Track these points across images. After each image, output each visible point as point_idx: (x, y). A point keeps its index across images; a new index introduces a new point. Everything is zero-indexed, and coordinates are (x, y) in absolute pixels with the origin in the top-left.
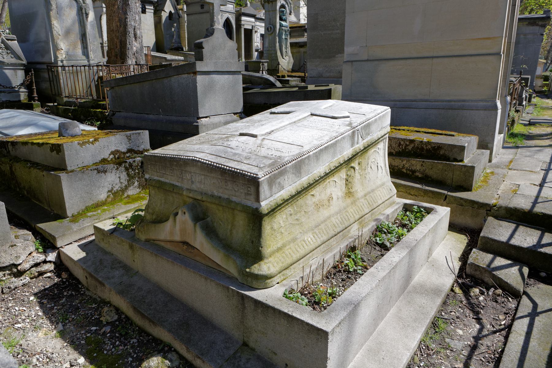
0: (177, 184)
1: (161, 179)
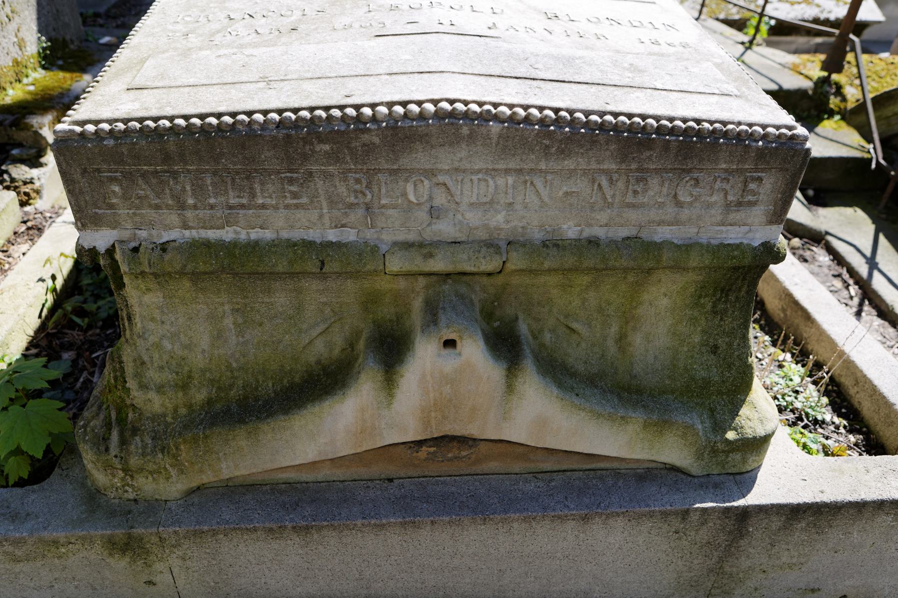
0: (332, 236)
1: (212, 234)
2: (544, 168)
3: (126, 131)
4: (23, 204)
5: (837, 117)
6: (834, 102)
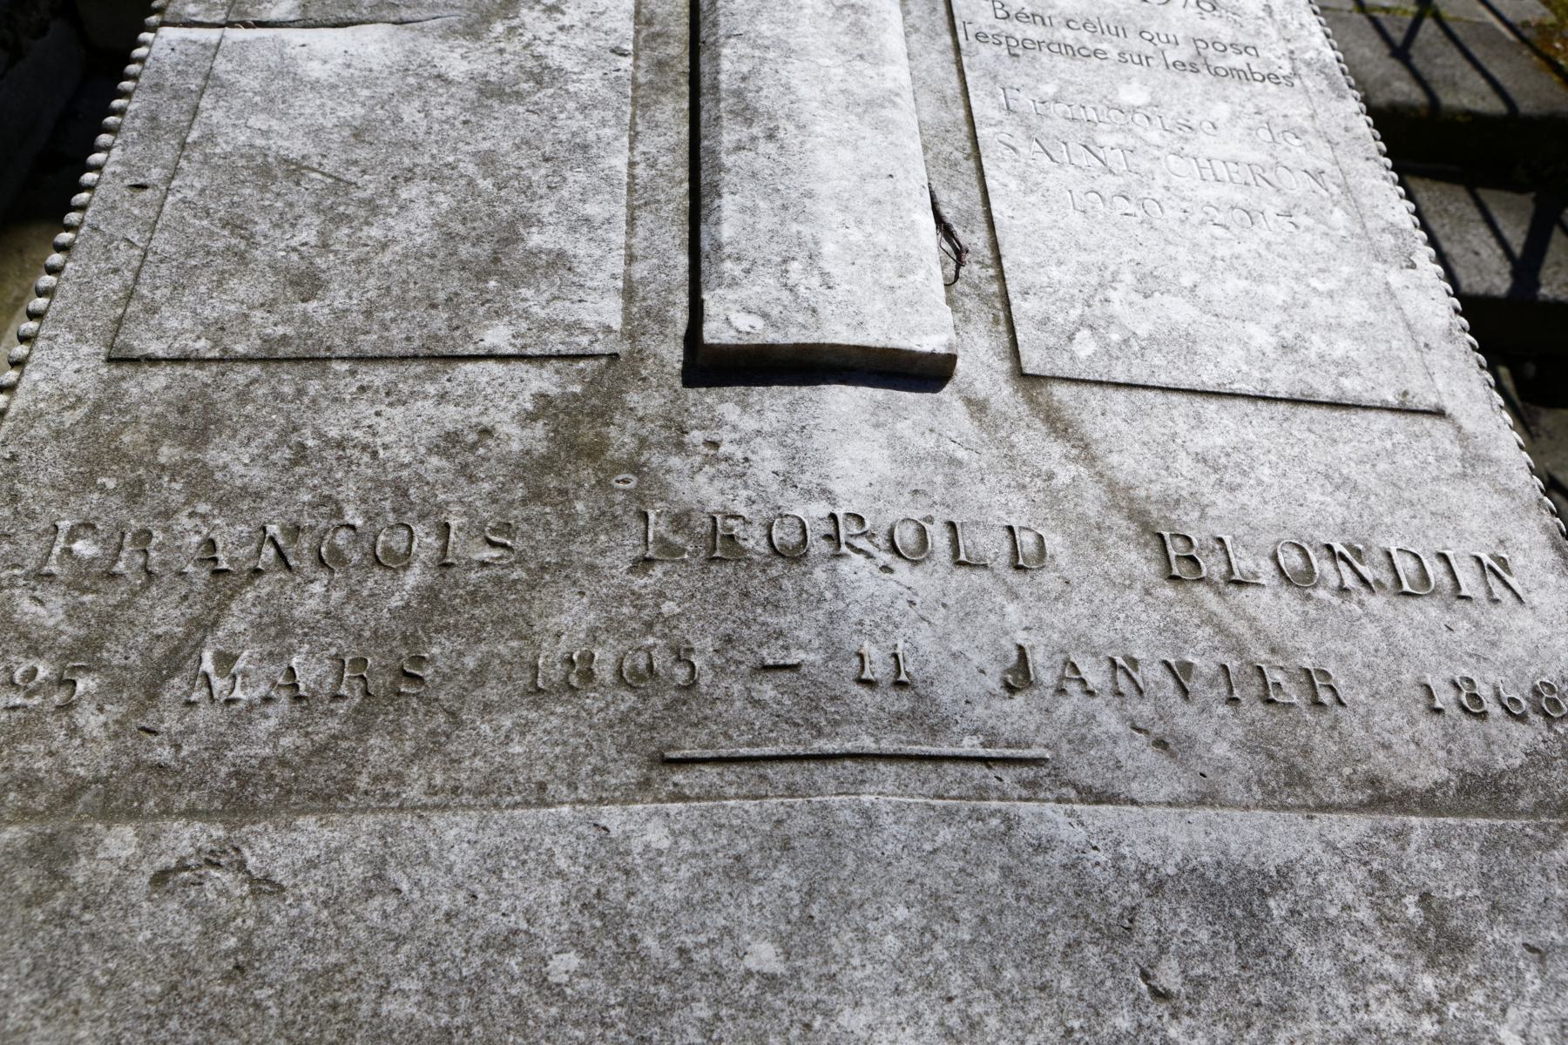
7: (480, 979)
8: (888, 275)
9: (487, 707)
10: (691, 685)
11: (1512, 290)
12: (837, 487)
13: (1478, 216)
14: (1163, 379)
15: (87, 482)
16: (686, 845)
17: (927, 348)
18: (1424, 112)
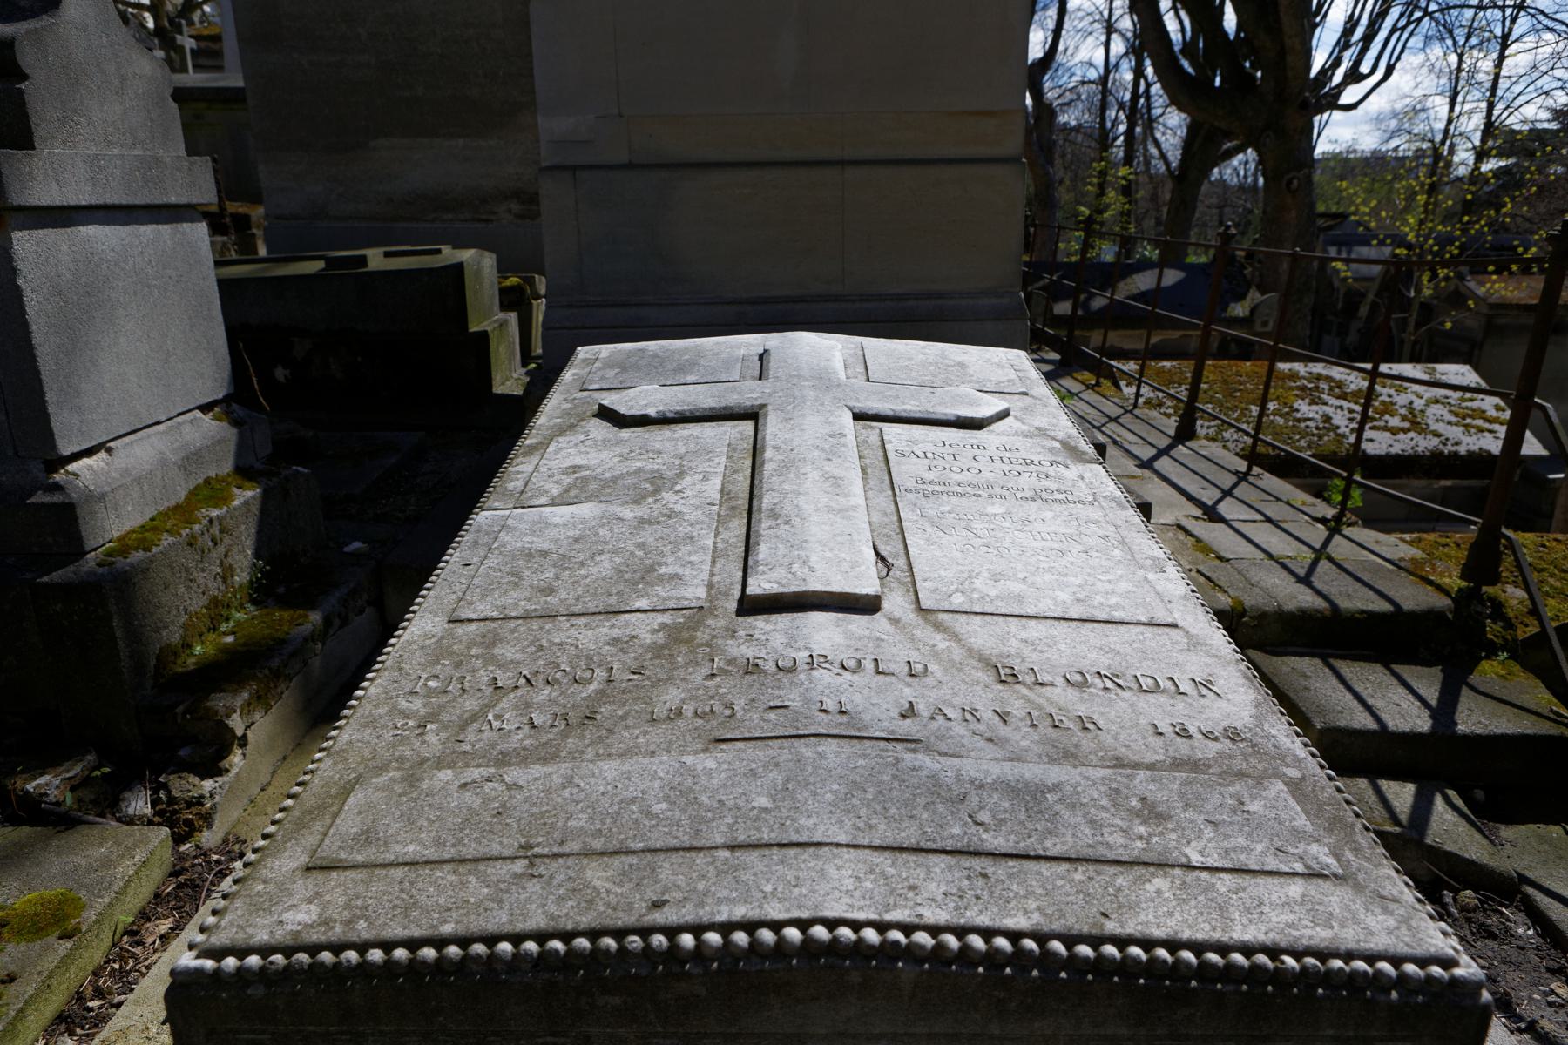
2: (997, 1032)
3: (287, 968)
4: (178, 839)
5: (1503, 656)
6: (1493, 629)
7: (618, 813)
8: (845, 567)
9: (627, 727)
10: (733, 715)
11: (1433, 727)
12: (813, 646)
13: (1395, 682)
14: (1003, 611)
15: (437, 662)
16: (725, 766)
17: (864, 591)
18: (1328, 613)
